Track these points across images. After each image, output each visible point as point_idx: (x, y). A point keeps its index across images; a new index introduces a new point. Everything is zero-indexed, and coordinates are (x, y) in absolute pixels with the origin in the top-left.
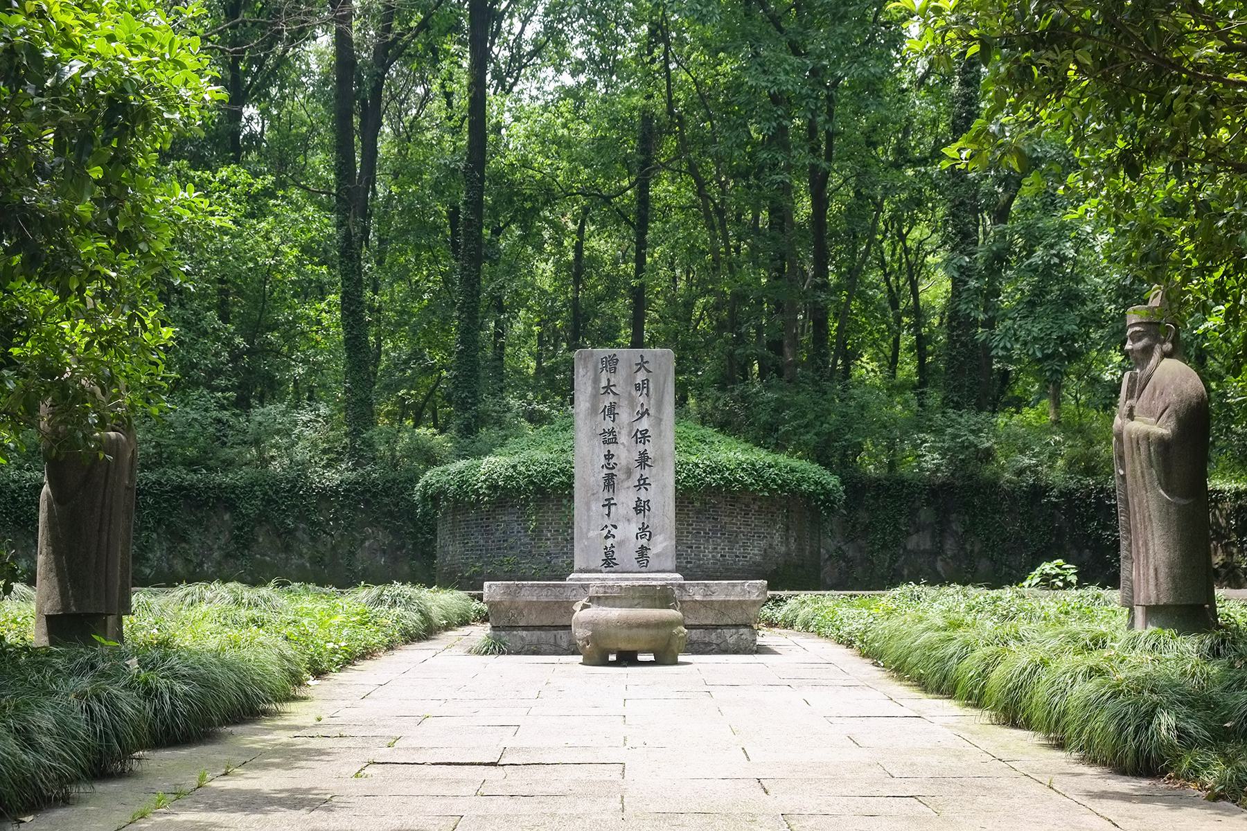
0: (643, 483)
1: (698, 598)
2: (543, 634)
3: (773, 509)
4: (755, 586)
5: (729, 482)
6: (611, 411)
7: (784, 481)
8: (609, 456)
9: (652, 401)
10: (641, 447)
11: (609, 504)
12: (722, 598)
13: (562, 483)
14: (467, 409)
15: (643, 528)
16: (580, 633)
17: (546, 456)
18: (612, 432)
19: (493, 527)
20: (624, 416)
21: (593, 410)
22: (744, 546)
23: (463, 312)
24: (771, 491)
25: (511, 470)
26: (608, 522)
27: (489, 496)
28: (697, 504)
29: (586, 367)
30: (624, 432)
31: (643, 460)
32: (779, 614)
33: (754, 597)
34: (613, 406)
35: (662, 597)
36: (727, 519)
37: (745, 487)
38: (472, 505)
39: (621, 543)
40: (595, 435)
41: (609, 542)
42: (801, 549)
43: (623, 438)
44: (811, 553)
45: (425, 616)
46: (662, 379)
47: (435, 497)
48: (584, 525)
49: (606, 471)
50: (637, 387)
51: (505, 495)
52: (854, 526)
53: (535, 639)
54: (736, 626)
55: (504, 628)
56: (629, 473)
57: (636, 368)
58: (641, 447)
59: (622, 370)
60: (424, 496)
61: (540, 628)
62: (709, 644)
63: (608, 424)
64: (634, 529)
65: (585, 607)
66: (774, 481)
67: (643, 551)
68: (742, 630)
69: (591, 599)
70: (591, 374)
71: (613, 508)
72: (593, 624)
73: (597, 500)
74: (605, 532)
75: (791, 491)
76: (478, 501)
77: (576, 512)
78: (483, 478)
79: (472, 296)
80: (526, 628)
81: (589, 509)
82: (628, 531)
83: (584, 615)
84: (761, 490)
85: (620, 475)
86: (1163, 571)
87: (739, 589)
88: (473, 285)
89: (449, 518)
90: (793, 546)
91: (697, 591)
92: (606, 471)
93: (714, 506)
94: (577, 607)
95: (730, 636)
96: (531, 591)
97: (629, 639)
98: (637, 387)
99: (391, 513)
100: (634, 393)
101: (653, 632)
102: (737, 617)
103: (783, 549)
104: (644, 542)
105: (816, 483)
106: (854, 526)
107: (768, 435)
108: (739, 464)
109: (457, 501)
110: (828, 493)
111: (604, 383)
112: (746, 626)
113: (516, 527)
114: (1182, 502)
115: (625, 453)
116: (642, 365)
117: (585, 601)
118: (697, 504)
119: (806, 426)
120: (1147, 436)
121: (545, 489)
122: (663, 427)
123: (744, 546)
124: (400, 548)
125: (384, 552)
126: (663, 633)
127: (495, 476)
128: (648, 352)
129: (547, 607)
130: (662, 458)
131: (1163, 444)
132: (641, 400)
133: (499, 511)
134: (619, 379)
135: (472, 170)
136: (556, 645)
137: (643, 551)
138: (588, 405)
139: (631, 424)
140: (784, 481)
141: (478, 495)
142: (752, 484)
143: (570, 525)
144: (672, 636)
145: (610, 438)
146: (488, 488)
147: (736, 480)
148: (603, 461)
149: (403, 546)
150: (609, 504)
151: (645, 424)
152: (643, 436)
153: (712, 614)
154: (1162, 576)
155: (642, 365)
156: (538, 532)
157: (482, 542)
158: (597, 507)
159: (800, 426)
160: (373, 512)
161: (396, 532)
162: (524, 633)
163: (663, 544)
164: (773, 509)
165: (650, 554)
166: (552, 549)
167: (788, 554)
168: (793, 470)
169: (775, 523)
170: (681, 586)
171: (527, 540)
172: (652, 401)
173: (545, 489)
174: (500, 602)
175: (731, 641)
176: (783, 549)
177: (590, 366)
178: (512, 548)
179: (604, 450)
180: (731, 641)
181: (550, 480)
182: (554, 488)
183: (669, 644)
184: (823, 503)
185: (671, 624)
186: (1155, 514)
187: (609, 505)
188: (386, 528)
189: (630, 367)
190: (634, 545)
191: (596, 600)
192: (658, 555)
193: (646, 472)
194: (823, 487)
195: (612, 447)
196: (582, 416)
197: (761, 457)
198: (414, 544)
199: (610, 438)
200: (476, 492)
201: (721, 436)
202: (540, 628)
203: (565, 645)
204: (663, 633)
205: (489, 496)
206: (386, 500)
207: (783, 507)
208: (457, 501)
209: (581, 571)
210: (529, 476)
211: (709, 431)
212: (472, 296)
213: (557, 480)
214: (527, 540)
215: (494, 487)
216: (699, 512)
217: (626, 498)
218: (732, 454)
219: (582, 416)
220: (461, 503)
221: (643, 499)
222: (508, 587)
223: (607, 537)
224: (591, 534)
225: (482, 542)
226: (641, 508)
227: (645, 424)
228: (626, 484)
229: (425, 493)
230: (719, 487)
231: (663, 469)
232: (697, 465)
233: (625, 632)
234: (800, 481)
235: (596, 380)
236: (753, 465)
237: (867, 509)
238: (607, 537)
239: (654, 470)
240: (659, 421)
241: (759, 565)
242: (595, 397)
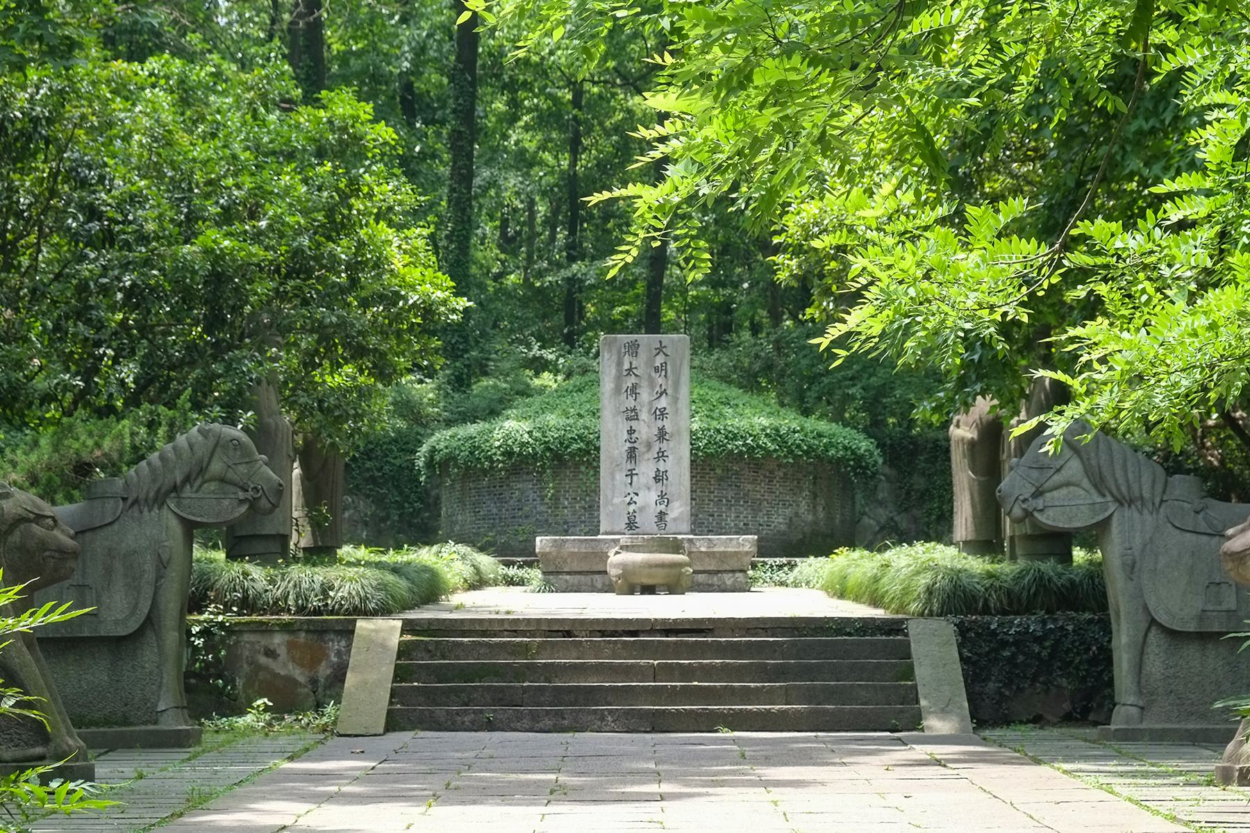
0: (661, 455)
1: (703, 549)
2: (583, 578)
3: (800, 476)
4: (746, 540)
5: (751, 449)
6: (634, 390)
7: (809, 447)
8: (631, 431)
9: (670, 382)
10: (660, 424)
11: (631, 474)
12: (722, 549)
13: (580, 449)
14: (457, 357)
15: (662, 496)
16: (613, 572)
17: (563, 421)
18: (634, 410)
19: (507, 495)
20: (645, 395)
21: (617, 390)
22: (768, 515)
23: (452, 242)
24: (796, 457)
25: (526, 436)
26: (630, 490)
27: (502, 462)
28: (719, 471)
29: (610, 351)
30: (645, 409)
31: (662, 434)
32: (791, 577)
33: (746, 549)
34: (635, 387)
35: (676, 547)
36: (749, 487)
37: (768, 453)
38: (485, 472)
39: (642, 509)
40: (618, 413)
41: (632, 508)
42: (830, 518)
43: (644, 415)
44: (842, 522)
45: (478, 571)
46: (678, 362)
47: (441, 465)
48: (609, 493)
49: (628, 445)
50: (656, 370)
51: (519, 462)
52: (908, 493)
53: (576, 582)
54: (733, 571)
55: (551, 573)
56: (649, 446)
57: (655, 352)
58: (660, 424)
59: (643, 355)
60: (430, 463)
61: (580, 573)
62: (712, 585)
63: (631, 403)
64: (653, 496)
65: (617, 553)
66: (799, 446)
67: (661, 516)
68: (738, 575)
69: (621, 548)
70: (615, 358)
71: (635, 478)
72: (624, 566)
73: (621, 470)
74: (628, 499)
75: (817, 457)
76: (491, 468)
77: (602, 481)
78: (497, 444)
79: (463, 222)
80: (569, 573)
81: (613, 478)
82: (648, 498)
83: (617, 559)
84: (785, 457)
85: (641, 448)
86: (970, 520)
87: (734, 542)
88: (463, 210)
89: (458, 486)
90: (821, 515)
91: (701, 544)
92: (628, 445)
93: (737, 473)
94: (611, 553)
95: (728, 579)
96: (574, 542)
97: (649, 576)
98: (656, 370)
99: (373, 480)
100: (653, 374)
101: (667, 570)
102: (734, 564)
103: (810, 518)
104: (662, 508)
105: (845, 448)
106: (908, 493)
107: (195, 824)
108: (763, 430)
109: (468, 468)
110: (859, 459)
111: (626, 366)
112: (741, 571)
113: (532, 496)
114: (982, 479)
115: (646, 429)
116: (660, 350)
117: (617, 549)
118: (719, 471)
119: (852, 379)
120: (963, 439)
121: (562, 455)
122: (679, 405)
123: (768, 515)
124: (383, 520)
125: (366, 524)
126: (674, 571)
127: (510, 442)
128: (666, 338)
129: (585, 557)
130: (679, 432)
131: (972, 444)
132: (660, 381)
133: (513, 478)
134: (640, 362)
135: (462, 72)
136: (593, 586)
137: (661, 516)
138: (612, 385)
139: (651, 403)
140: (809, 447)
141: (492, 461)
142: (775, 450)
143: (596, 491)
144: (681, 574)
145: (632, 414)
146: (503, 454)
147: (758, 446)
148: (626, 436)
149: (388, 517)
150: (631, 474)
151: (663, 402)
152: (662, 413)
153: (714, 562)
154: (969, 523)
155: (660, 350)
156: (555, 498)
157: (495, 511)
158: (620, 477)
159: (845, 378)
160: (353, 478)
161: (379, 501)
162: (568, 577)
163: (679, 510)
164: (800, 476)
165: (668, 518)
166: (570, 518)
167: (815, 523)
168: (820, 435)
169: (801, 490)
170: (690, 541)
171: (543, 508)
172: (670, 382)
173: (562, 455)
174: (549, 553)
175: (729, 582)
176: (810, 518)
177: (614, 351)
178: (527, 517)
179: (625, 426)
180: (729, 582)
181: (567, 447)
182: (572, 455)
183: (679, 580)
184: (854, 468)
185: (681, 565)
186: (966, 486)
187: (632, 475)
188: (368, 496)
189: (650, 351)
190: (654, 510)
191: (625, 548)
192: (675, 519)
193: (664, 446)
194: (853, 452)
195: (634, 424)
196: (607, 395)
197: (790, 421)
198: (400, 516)
199: (632, 414)
200: (490, 459)
201: (746, 398)
202: (580, 573)
203: (599, 586)
204: (674, 571)
205: (502, 462)
206: (368, 464)
207: (810, 473)
208: (468, 468)
209: (607, 533)
210: (546, 442)
211: (735, 392)
212: (463, 222)
213: (575, 446)
214: (543, 508)
215: (509, 454)
216: (721, 479)
217: (646, 469)
218: (757, 419)
219: (607, 395)
220: (472, 469)
221: (662, 469)
222: (555, 541)
223: (629, 504)
224: (616, 501)
225: (495, 511)
226: (659, 478)
227: (663, 402)
228: (646, 456)
229: (432, 457)
230: (741, 453)
231: (680, 443)
232: (718, 431)
233: (648, 570)
234: (827, 447)
235: (620, 364)
236: (777, 430)
237: (923, 474)
238: (629, 504)
239: (671, 444)
240: (676, 400)
241: (784, 534)
242: (619, 378)
